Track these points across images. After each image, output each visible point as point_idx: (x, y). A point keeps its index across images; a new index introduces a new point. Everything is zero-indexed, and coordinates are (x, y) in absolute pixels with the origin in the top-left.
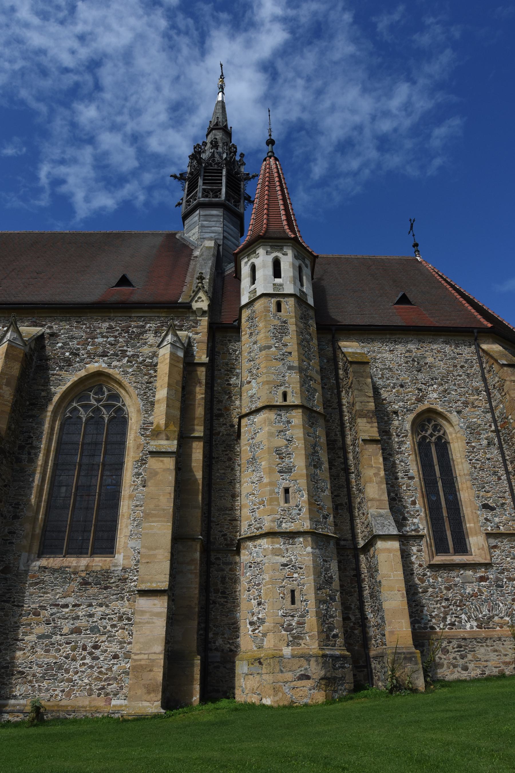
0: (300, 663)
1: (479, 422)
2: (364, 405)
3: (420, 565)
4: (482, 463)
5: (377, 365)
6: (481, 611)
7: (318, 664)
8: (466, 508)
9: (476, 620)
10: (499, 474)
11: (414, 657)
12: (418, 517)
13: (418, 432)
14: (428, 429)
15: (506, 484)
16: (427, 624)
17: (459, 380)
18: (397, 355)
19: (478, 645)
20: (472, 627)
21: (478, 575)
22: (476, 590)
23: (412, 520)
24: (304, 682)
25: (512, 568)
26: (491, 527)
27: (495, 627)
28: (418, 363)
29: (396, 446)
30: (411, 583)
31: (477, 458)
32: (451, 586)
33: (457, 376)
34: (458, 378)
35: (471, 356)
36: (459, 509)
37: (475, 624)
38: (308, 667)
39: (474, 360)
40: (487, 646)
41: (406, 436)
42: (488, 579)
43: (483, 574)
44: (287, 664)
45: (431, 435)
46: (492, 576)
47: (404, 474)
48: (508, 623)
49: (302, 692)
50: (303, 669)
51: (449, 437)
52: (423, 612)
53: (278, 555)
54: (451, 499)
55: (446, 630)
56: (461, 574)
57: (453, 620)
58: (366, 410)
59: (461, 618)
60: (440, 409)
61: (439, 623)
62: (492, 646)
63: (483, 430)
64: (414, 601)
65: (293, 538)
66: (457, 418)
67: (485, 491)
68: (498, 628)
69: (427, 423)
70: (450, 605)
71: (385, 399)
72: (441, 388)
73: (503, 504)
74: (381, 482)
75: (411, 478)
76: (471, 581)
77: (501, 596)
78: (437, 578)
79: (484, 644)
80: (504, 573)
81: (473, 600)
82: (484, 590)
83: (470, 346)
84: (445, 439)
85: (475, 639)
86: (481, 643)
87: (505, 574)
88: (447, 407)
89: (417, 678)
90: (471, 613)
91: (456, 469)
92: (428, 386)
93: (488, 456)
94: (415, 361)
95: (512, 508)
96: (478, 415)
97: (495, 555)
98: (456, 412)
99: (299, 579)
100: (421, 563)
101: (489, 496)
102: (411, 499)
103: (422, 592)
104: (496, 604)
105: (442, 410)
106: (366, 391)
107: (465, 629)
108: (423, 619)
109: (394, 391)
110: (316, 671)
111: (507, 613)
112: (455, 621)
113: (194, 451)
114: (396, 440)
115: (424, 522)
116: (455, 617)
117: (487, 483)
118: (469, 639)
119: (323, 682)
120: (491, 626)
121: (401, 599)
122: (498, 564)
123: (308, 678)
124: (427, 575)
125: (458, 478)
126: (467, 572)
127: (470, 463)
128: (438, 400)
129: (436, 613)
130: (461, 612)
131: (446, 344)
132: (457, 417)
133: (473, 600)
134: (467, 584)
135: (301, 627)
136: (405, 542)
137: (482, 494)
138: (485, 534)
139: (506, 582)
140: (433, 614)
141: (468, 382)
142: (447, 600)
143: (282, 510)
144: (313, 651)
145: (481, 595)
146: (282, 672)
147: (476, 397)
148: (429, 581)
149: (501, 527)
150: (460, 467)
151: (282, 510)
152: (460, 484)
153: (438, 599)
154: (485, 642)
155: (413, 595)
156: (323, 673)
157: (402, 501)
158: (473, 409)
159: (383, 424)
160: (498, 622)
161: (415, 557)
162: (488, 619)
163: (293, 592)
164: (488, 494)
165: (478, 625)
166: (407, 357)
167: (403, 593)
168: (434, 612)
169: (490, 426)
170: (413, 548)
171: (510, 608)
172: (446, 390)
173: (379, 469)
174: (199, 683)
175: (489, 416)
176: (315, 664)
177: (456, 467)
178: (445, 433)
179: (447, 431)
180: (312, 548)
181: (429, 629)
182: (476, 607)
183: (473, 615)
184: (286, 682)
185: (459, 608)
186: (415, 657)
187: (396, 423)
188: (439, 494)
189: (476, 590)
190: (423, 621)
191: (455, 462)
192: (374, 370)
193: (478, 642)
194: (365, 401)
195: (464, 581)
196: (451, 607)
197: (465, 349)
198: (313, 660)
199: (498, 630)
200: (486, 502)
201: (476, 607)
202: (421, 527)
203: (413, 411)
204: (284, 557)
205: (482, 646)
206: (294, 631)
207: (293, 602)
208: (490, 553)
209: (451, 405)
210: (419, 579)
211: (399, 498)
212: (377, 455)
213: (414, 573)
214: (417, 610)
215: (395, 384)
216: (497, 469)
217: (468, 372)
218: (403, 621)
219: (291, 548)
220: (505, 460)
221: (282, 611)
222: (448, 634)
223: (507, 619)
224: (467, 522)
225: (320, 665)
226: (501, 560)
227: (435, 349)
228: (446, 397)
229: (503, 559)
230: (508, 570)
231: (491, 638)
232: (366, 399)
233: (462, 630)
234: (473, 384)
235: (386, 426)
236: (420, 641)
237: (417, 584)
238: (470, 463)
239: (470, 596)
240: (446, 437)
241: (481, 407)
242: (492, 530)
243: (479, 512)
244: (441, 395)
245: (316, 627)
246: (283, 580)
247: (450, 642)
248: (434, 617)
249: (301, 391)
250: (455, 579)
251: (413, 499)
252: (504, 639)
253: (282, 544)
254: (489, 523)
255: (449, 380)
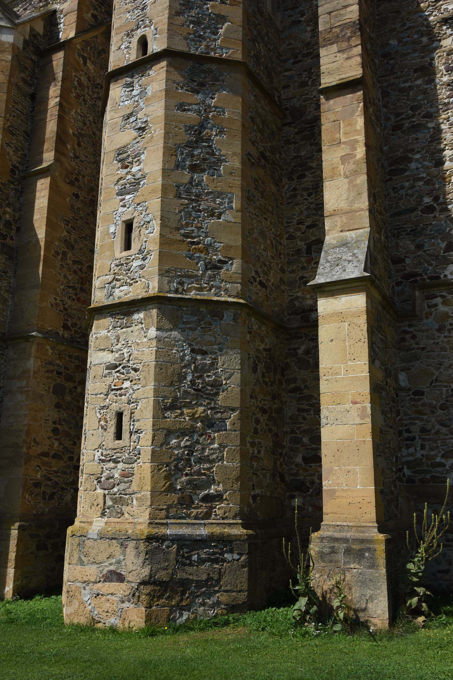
0: (111, 550)
7: (138, 555)
11: (369, 549)
24: (114, 586)
38: (122, 558)
44: (90, 550)
49: (108, 604)
50: (114, 561)
53: (104, 350)
65: (129, 314)
74: (355, 173)
89: (371, 598)
99: (131, 391)
110: (134, 568)
113: (38, 194)
119: (147, 589)
121: (358, 420)
123: (120, 578)
135: (125, 483)
143: (117, 266)
144: (139, 527)
146: (81, 563)
151: (117, 266)
156: (146, 571)
159: (417, 54)
163: (120, 415)
167: (364, 408)
173: (353, 144)
174: (13, 566)
176: (133, 553)
180: (158, 329)
184: (87, 582)
186: (372, 551)
198: (132, 544)
204: (112, 352)
206: (115, 489)
207: (118, 436)
218: (358, 469)
219: (124, 333)
221: (100, 450)
225: (142, 556)
235: (423, 57)
245: (149, 483)
246: (107, 395)
249: (170, 24)
253: (111, 328)
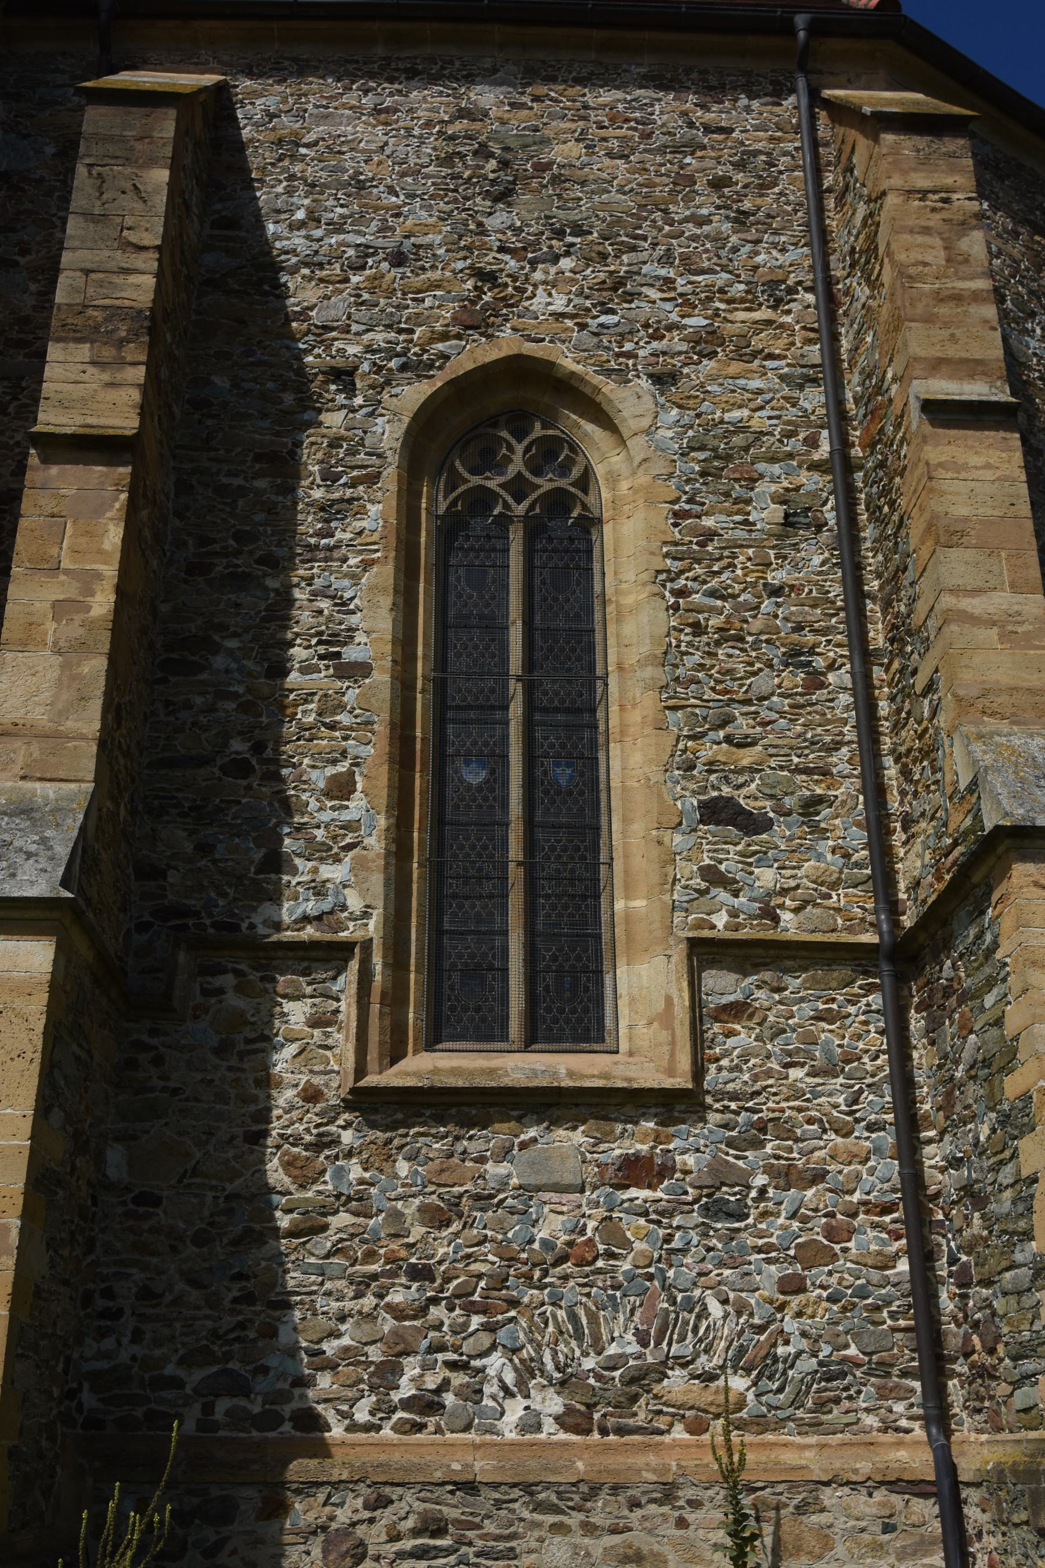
1: (759, 421)
2: (101, 284)
3: (311, 1095)
4: (738, 608)
5: (297, 168)
6: (596, 1338)
8: (626, 821)
9: (563, 1383)
10: (819, 663)
12: (348, 858)
13: (453, 470)
14: (510, 460)
15: (847, 709)
16: (285, 1397)
17: (694, 238)
18: (409, 130)
19: (538, 1525)
20: (531, 1423)
21: (617, 1151)
22: (591, 1225)
23: (315, 871)
25: (810, 1121)
26: (734, 913)
27: (661, 1423)
28: (504, 164)
29: (309, 524)
30: (238, 1182)
31: (714, 583)
32: (455, 1203)
33: (686, 220)
34: (691, 229)
35: (771, 139)
36: (597, 829)
37: (552, 1404)
39: (785, 154)
40: (589, 1529)
41: (372, 479)
42: (666, 1171)
43: (644, 1148)
45: (518, 488)
46: (690, 1160)
47: (321, 650)
48: (741, 1404)
51: (605, 495)
52: (274, 1333)
54: (563, 782)
55: (387, 1432)
56: (523, 1146)
57: (431, 1382)
58: (105, 308)
59: (482, 1370)
60: (569, 363)
61: (350, 1393)
62: (614, 1531)
63: (773, 460)
64: (240, 1277)
66: (648, 402)
67: (728, 739)
68: (679, 1433)
69: (504, 434)
70: (434, 1301)
71: (303, 315)
72: (595, 274)
73: (811, 805)
75: (357, 671)
76: (568, 1179)
77: (721, 1264)
78: (390, 1158)
79: (574, 1520)
80: (760, 1144)
81: (565, 1278)
82: (633, 1226)
83: (778, 92)
84: (585, 507)
85: (528, 1488)
86: (557, 1510)
87: (769, 1149)
88: (605, 355)
90: (539, 1347)
91: (611, 641)
92: (534, 263)
93: (776, 577)
94: (491, 155)
95: (858, 825)
96: (759, 392)
97: (727, 1053)
98: (650, 376)
100: (317, 1080)
101: (745, 762)
102: (330, 771)
103: (292, 1234)
104: (689, 1305)
105: (578, 368)
106: (129, 221)
107: (491, 1430)
108: (265, 1370)
109: (355, 279)
111: (742, 1351)
112: (444, 1386)
114: (318, 494)
115: (377, 881)
116: (452, 1366)
117: (747, 702)
118: (495, 1486)
120: (641, 1419)
122: (734, 1097)
124: (336, 1142)
125: (612, 681)
126: (561, 1133)
127: (676, 607)
128: (569, 323)
129: (346, 1341)
130: (486, 1339)
131: (660, 87)
132: (647, 399)
133: (565, 1278)
134: (547, 1196)
136: (254, 976)
137: (707, 751)
138: (683, 946)
139: (762, 1191)
140: (330, 1347)
141: (735, 250)
142: (421, 1274)
145: (610, 1255)
147: (764, 314)
148: (340, 1174)
149: (786, 916)
150: (629, 629)
152: (614, 709)
153: (375, 1268)
154: (578, 1509)
155: (236, 1242)
157: (282, 780)
158: (735, 367)
159: (267, 424)
160: (680, 1399)
161: (292, 1049)
162: (632, 1380)
164: (742, 751)
165: (569, 1410)
166: (452, 138)
168: (339, 1335)
169: (812, 442)
170: (288, 1006)
171: (761, 1329)
172: (620, 283)
173: (88, 581)
175: (813, 399)
177: (611, 629)
178: (585, 481)
179: (600, 470)
181: (287, 1427)
182: (573, 1318)
183: (547, 1358)
185: (476, 1321)
187: (334, 420)
188: (505, 757)
189: (591, 1225)
190: (261, 1384)
191: (610, 609)
192: (280, 189)
193: (540, 1507)
194: (112, 265)
195: (533, 1181)
196: (437, 1312)
197: (748, 109)
199: (675, 1445)
200: (726, 791)
201: (573, 1318)
202: (354, 902)
203: (431, 366)
205: (558, 1528)
208: (698, 1041)
209: (628, 346)
210: (289, 1165)
211: (268, 761)
212: (99, 511)
213: (266, 1133)
214: (242, 1326)
215: (365, 251)
216: (810, 638)
217: (747, 205)
220: (857, 594)
222: (383, 1457)
223: (739, 1383)
224: (618, 893)
226: (755, 1078)
227: (603, 107)
228: (613, 312)
229: (769, 1074)
230: (787, 1133)
231: (615, 1489)
232: (122, 259)
233: (472, 1436)
234: (760, 259)
235: (278, 434)
236: (215, 1492)
237: (272, 1190)
238: (676, 607)
239: (550, 1258)
240: (591, 500)
241: (779, 357)
242: (737, 928)
243: (678, 838)
244: (588, 303)
247: (382, 1502)
248: (332, 1366)
250: (489, 1166)
251: (342, 767)
252: (689, 1493)
254: (723, 895)
255: (645, 238)
